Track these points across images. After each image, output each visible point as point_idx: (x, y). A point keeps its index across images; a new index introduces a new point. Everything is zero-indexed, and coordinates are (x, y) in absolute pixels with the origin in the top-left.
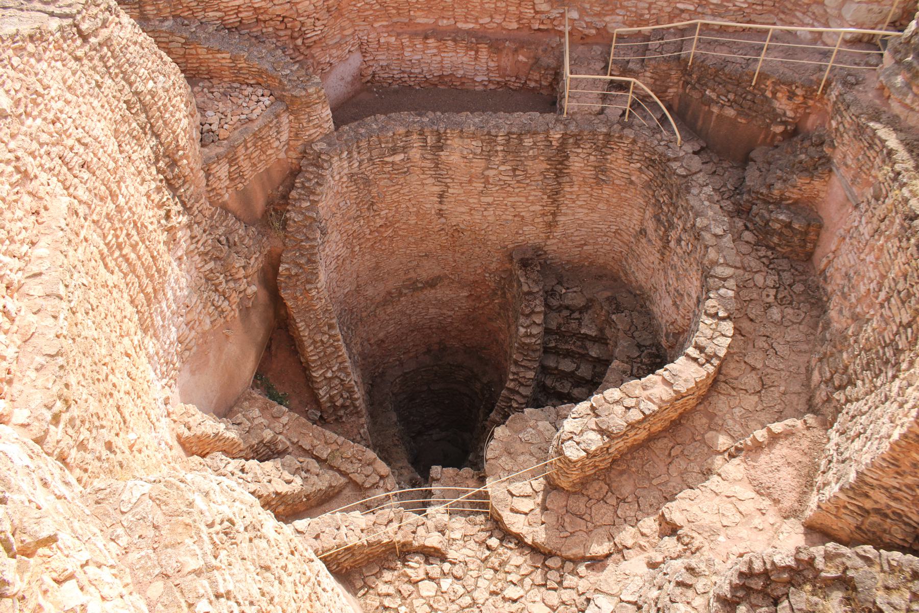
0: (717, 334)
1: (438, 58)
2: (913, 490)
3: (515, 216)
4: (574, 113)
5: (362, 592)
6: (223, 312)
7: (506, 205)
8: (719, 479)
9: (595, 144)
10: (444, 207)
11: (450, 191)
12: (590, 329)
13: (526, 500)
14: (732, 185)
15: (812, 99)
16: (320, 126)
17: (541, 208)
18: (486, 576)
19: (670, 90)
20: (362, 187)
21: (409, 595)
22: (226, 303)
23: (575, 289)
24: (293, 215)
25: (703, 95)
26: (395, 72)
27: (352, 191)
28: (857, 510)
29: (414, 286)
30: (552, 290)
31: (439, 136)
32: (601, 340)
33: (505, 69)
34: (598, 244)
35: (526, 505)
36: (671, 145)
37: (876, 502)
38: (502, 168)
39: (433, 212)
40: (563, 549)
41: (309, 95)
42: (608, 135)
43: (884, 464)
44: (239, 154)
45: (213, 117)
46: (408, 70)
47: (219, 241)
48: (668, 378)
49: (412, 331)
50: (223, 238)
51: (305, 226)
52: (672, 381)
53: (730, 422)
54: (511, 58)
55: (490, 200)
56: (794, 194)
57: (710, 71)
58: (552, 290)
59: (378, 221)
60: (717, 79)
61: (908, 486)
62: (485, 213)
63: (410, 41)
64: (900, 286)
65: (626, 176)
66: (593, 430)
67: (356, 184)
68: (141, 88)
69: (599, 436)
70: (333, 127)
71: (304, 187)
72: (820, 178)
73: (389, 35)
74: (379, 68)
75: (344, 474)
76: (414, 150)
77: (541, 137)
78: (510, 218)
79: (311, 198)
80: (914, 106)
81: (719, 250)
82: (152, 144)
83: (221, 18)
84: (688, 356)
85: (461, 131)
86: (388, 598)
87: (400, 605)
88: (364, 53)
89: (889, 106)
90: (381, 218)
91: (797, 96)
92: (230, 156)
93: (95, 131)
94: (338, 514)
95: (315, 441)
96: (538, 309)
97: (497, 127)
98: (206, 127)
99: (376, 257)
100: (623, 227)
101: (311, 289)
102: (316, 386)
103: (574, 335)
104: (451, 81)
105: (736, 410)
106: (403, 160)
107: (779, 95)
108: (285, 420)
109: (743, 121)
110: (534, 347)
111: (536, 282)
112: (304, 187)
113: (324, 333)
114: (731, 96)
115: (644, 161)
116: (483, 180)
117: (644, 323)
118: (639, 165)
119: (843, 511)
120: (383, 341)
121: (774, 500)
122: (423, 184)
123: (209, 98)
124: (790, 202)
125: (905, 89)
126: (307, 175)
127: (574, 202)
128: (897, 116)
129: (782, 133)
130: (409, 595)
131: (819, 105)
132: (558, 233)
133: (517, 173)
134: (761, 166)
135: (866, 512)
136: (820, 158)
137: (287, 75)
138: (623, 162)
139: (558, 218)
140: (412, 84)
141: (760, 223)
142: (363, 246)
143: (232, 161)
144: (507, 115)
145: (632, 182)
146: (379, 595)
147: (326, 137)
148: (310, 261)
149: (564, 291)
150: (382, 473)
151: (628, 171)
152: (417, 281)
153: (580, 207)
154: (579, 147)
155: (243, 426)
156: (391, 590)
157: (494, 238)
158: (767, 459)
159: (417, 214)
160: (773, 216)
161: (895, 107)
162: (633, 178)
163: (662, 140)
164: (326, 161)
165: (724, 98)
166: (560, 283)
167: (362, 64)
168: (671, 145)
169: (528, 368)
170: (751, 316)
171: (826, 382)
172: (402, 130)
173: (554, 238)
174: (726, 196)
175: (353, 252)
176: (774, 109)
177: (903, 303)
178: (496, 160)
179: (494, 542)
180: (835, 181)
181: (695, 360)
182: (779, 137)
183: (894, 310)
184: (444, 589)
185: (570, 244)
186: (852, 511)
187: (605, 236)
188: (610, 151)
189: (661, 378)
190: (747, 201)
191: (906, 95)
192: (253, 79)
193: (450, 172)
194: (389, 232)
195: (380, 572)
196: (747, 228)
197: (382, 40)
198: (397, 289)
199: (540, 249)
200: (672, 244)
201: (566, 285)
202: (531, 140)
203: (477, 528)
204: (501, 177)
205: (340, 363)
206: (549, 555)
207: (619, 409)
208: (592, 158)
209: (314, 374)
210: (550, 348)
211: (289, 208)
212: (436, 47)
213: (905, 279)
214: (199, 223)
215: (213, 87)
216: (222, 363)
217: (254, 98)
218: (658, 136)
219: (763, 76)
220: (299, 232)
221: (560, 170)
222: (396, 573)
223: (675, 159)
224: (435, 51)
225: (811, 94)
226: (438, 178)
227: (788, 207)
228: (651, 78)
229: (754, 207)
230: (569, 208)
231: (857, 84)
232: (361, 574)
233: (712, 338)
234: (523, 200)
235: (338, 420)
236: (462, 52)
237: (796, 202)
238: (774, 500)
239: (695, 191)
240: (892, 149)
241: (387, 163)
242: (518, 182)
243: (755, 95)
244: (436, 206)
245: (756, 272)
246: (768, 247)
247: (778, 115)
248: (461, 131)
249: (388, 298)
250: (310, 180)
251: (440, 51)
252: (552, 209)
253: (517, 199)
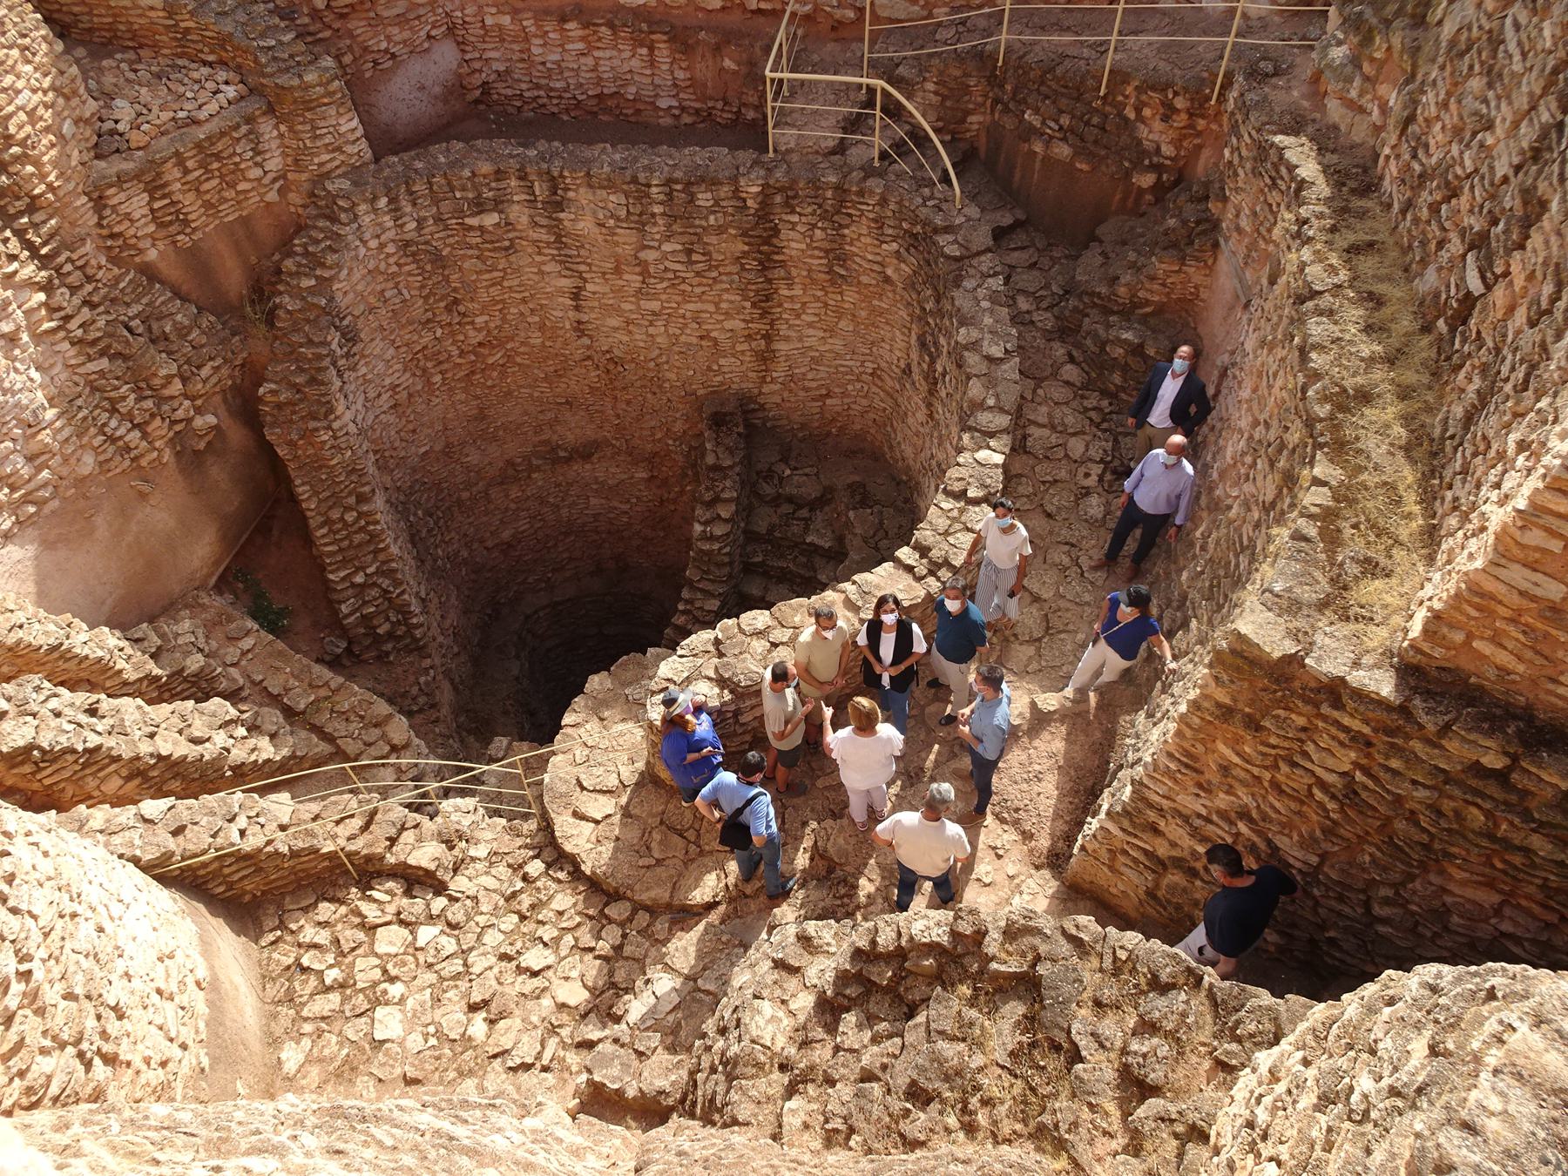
0: (958, 526)
2: (1232, 823)
3: (702, 338)
4: (789, 151)
5: (271, 937)
6: (128, 449)
7: (684, 317)
9: (820, 206)
10: (585, 318)
12: (822, 536)
13: (602, 799)
14: (1062, 287)
15: (1203, 116)
16: (339, 149)
17: (743, 325)
18: (503, 927)
19: (972, 119)
20: (428, 267)
21: (353, 949)
22: (137, 434)
23: (807, 470)
24: (287, 299)
25: (1022, 120)
26: (524, 86)
27: (410, 274)
28: (1142, 858)
29: (556, 456)
30: (770, 470)
31: (554, 183)
34: (849, 396)
35: (601, 807)
36: (944, 206)
37: (1173, 845)
38: (667, 247)
39: (568, 326)
40: (637, 887)
41: (306, 87)
42: (839, 188)
43: (1173, 766)
44: (167, 177)
45: (123, 110)
46: (543, 82)
48: (853, 597)
49: (567, 534)
51: (308, 321)
52: (860, 603)
54: (710, 63)
55: (655, 305)
56: (1153, 294)
57: (1032, 75)
58: (770, 470)
59: (472, 333)
60: (1043, 89)
61: (1223, 814)
62: (651, 330)
63: (539, 27)
65: (876, 267)
66: (709, 679)
67: (416, 261)
69: (717, 690)
70: (369, 155)
71: (306, 254)
72: (1197, 259)
73: (500, 12)
74: (493, 77)
75: (329, 739)
76: (516, 207)
77: (725, 190)
78: (695, 341)
79: (318, 272)
80: (1363, 101)
81: (990, 382)
85: (588, 174)
86: (312, 952)
87: (331, 966)
88: (461, 44)
89: (1322, 108)
90: (479, 330)
91: (1178, 111)
92: (148, 178)
94: (239, 795)
95: (291, 681)
96: (726, 495)
97: (650, 169)
98: (109, 125)
99: (477, 397)
100: (883, 365)
101: (317, 430)
102: (335, 597)
103: (796, 545)
104: (617, 106)
106: (498, 224)
107: (1147, 112)
108: (247, 643)
109: (1084, 167)
110: (719, 558)
111: (731, 451)
112: (306, 254)
113: (348, 509)
114: (1065, 120)
115: (903, 238)
116: (638, 269)
117: (901, 527)
118: (895, 246)
119: (1122, 859)
120: (509, 545)
121: (1024, 833)
122: (541, 273)
123: (127, 80)
124: (1148, 310)
125: (1349, 69)
126: (313, 233)
127: (798, 316)
128: (1336, 128)
130: (353, 949)
131: (1214, 127)
132: (779, 372)
133: (695, 257)
134: (1109, 249)
135: (1159, 865)
136: (1198, 223)
137: (270, 48)
138: (869, 240)
139: (776, 346)
140: (555, 110)
141: (1093, 348)
142: (449, 375)
143: (155, 188)
144: (673, 150)
145: (887, 280)
146: (300, 945)
147: (354, 173)
148: (313, 381)
149: (788, 472)
150: (395, 742)
151: (879, 259)
152: (558, 446)
153: (810, 325)
154: (793, 212)
155: (146, 644)
156: (323, 937)
157: (673, 376)
158: (1024, 757)
159: (542, 327)
160: (1113, 333)
161: (1335, 110)
162: (889, 272)
163: (932, 197)
164: (345, 210)
165: (1052, 124)
166: (784, 460)
167: (460, 66)
168: (944, 206)
169: (709, 594)
170: (1049, 508)
172: (486, 168)
173: (773, 380)
174: (1044, 304)
175: (429, 383)
176: (1139, 142)
178: (657, 230)
179: (535, 867)
180: (1224, 265)
181: (909, 569)
182: (1149, 197)
184: (420, 943)
185: (802, 394)
186: (1135, 860)
187: (858, 380)
188: (847, 221)
189: (843, 596)
190: (1075, 310)
191: (1349, 80)
192: (212, 52)
193: (582, 252)
194: (497, 357)
195: (315, 905)
196: (1072, 360)
197: (489, 21)
198: (524, 458)
199: (752, 399)
201: (793, 463)
202: (709, 195)
203: (519, 842)
204: (667, 263)
205: (383, 563)
206: (614, 896)
208: (818, 232)
209: (331, 577)
210: (754, 564)
211: (281, 288)
212: (582, 39)
215: (140, 61)
216: (129, 538)
217: (210, 85)
218: (926, 191)
219: (1119, 77)
220: (297, 331)
221: (768, 255)
222: (343, 910)
223: (948, 229)
224: (581, 46)
225: (1201, 106)
226: (565, 262)
227: (1144, 319)
228: (936, 93)
229: (1087, 320)
230: (791, 327)
231: (1275, 74)
232: (280, 906)
233: (946, 533)
234: (712, 308)
235: (382, 658)
236: (626, 48)
237: (1160, 310)
238: (1024, 833)
239: (969, 284)
240: (1303, 181)
241: (471, 228)
242: (698, 274)
243: (1106, 116)
244: (571, 314)
245: (1074, 434)
246: (1104, 393)
247: (1145, 153)
248: (588, 174)
249: (510, 472)
250: (317, 242)
251: (591, 48)
252: (762, 326)
253: (699, 306)
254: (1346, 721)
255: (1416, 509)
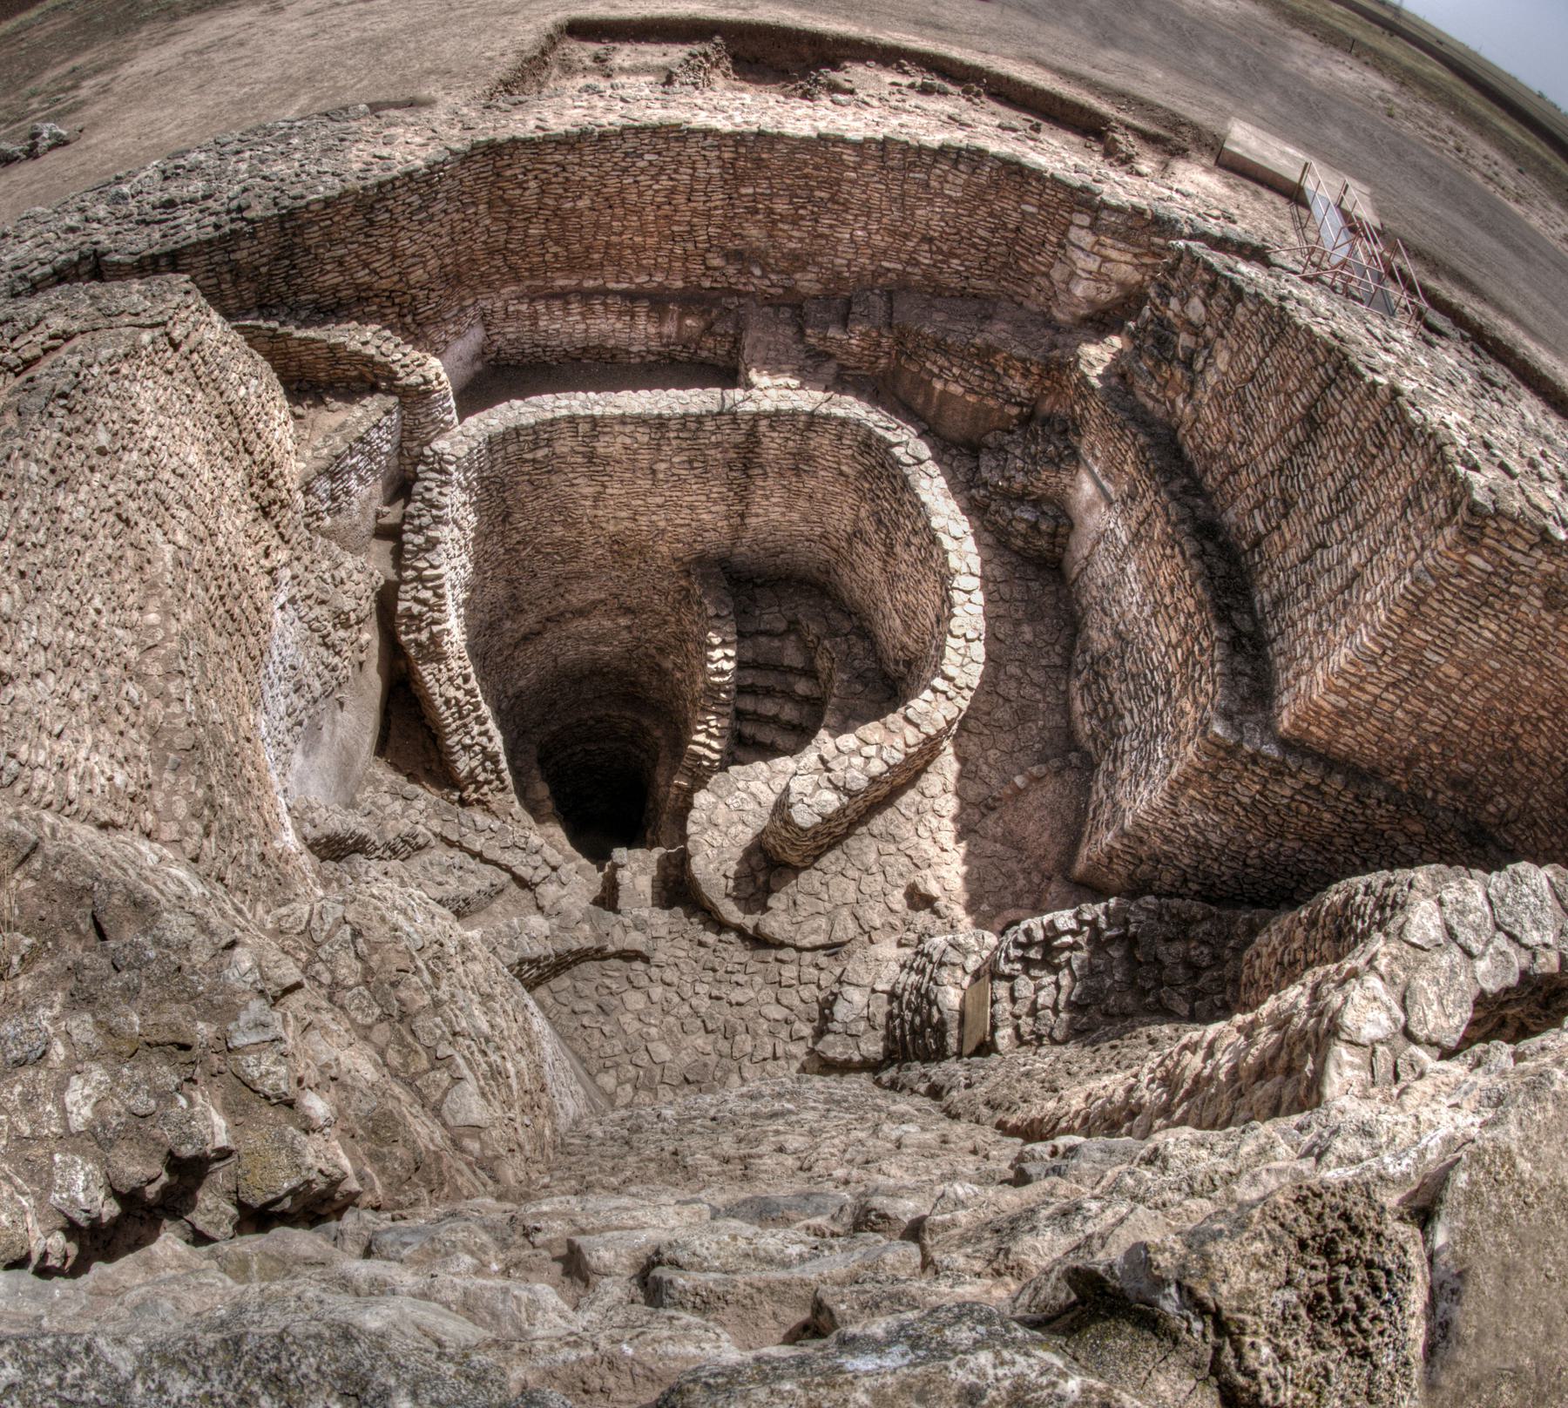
1: (583, 326)
8: (46, 362)
11: (609, 491)
32: (810, 673)
33: (669, 337)
38: (676, 460)
47: (324, 581)
50: (327, 576)
53: (985, 768)
64: (1167, 600)
68: (233, 396)
82: (245, 464)
83: (315, 301)
84: (935, 690)
88: (487, 327)
93: (1364, 1032)
105: (991, 752)
108: (420, 804)
129: (1016, 417)
139: (747, 521)
145: (841, 473)
153: (775, 505)
162: (844, 468)
170: (1001, 636)
171: (1090, 715)
177: (1171, 619)
183: (1162, 626)
197: (511, 309)
200: (898, 549)
207: (857, 761)
213: (1172, 592)
214: (298, 559)
234: (703, 498)
241: (527, 461)
254: (1258, 771)
255: (465, 110)
